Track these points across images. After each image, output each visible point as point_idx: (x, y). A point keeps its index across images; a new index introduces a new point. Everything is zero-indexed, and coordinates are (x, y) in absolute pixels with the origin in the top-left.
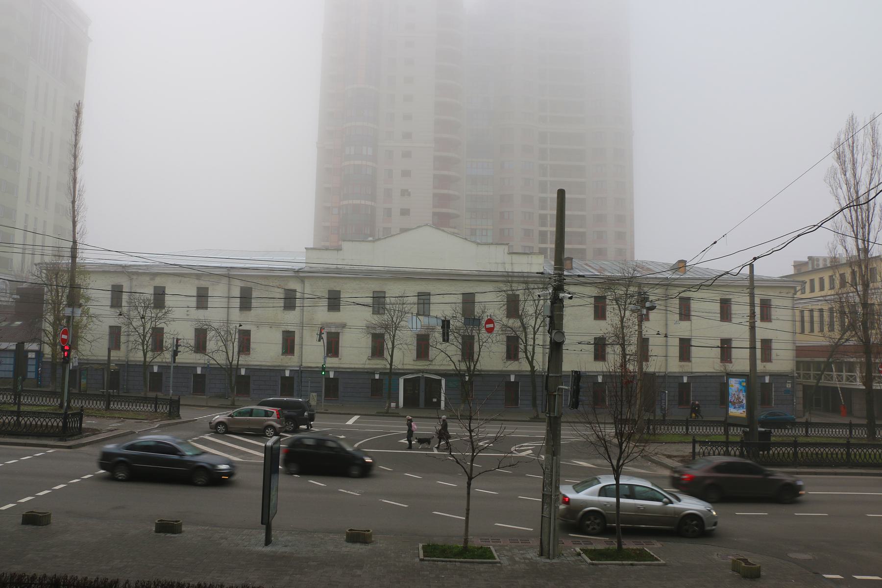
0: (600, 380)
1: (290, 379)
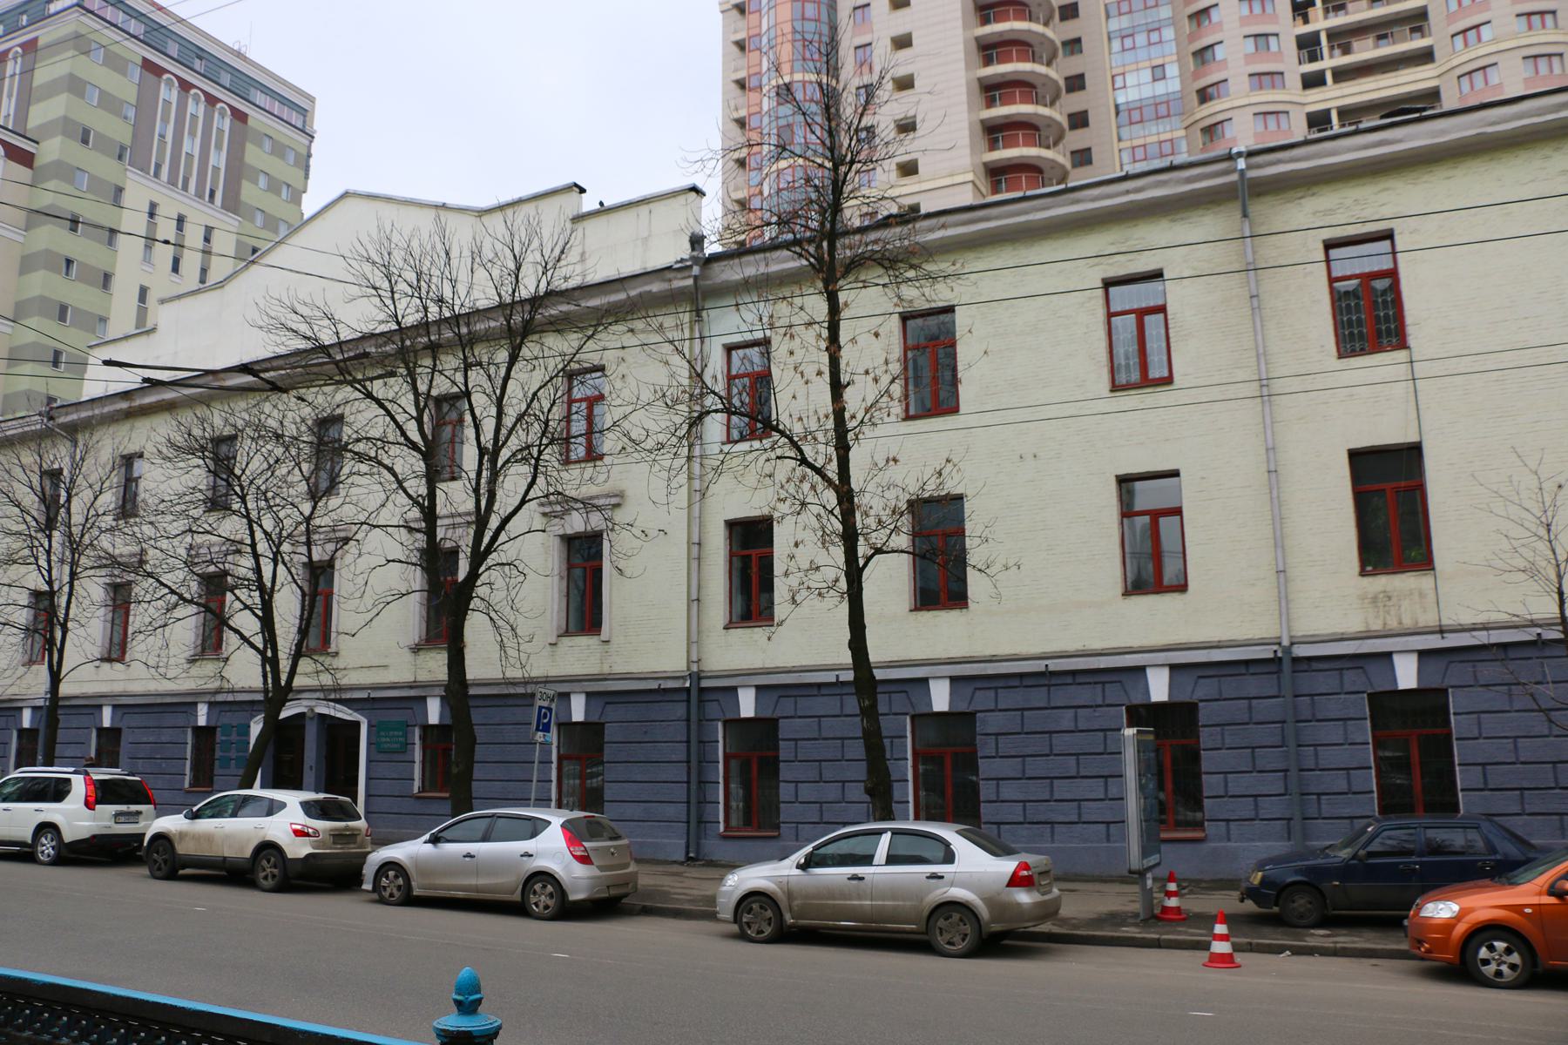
0: (940, 698)
1: (959, 721)
